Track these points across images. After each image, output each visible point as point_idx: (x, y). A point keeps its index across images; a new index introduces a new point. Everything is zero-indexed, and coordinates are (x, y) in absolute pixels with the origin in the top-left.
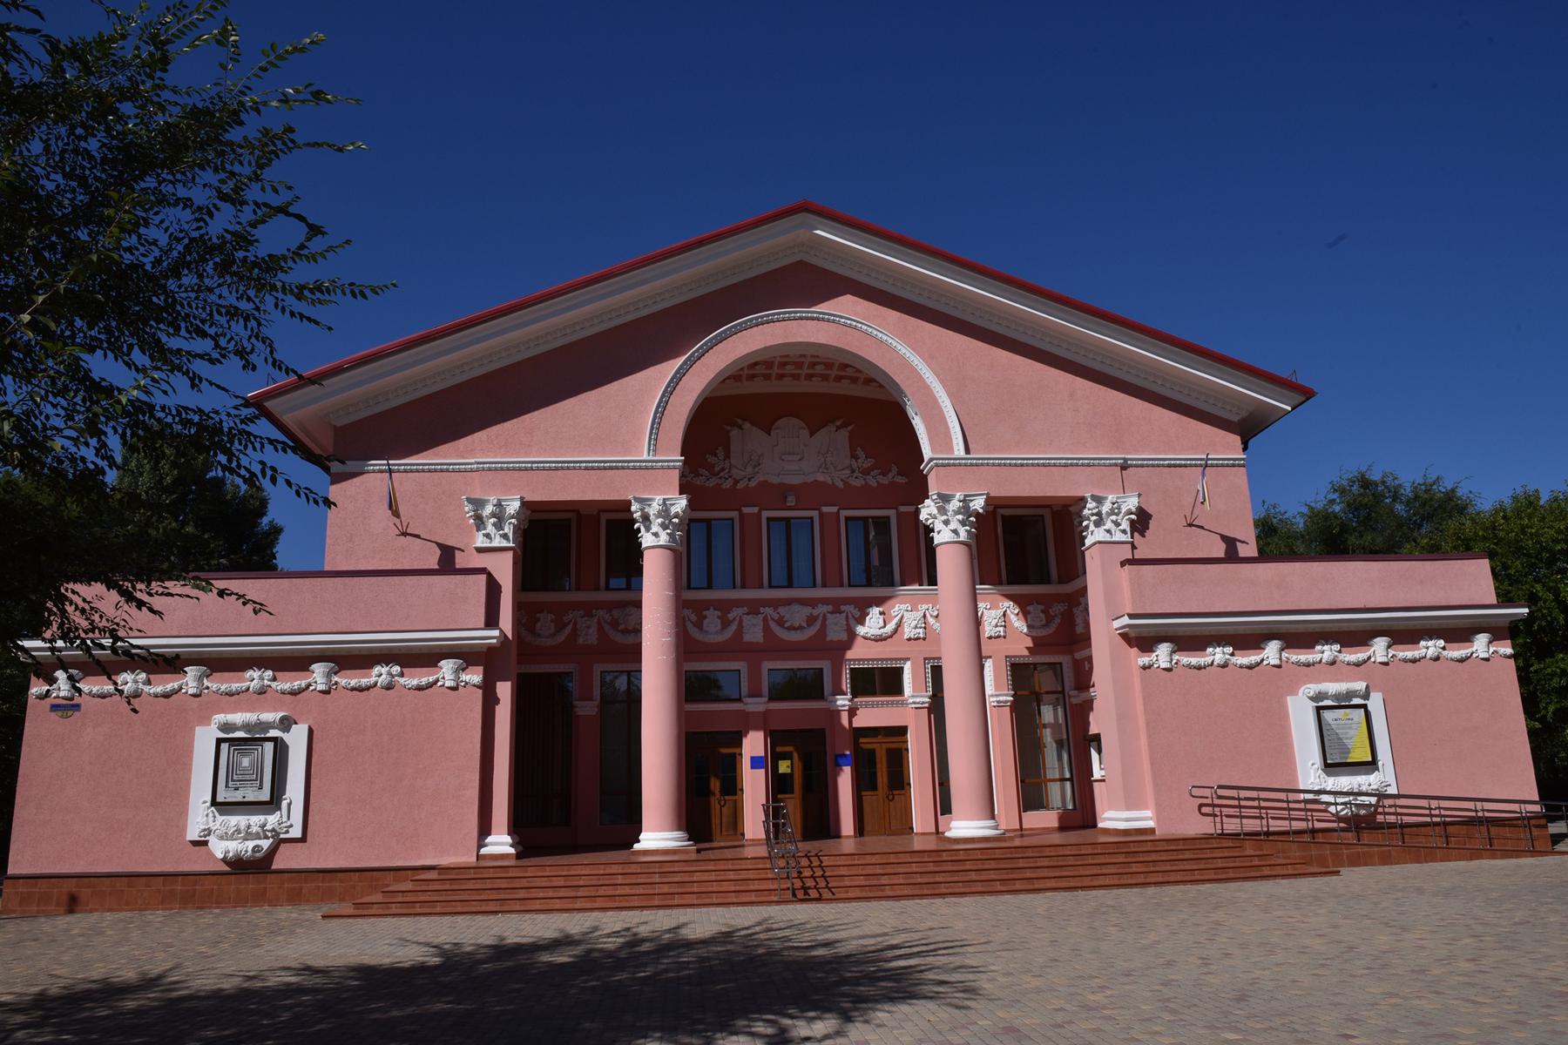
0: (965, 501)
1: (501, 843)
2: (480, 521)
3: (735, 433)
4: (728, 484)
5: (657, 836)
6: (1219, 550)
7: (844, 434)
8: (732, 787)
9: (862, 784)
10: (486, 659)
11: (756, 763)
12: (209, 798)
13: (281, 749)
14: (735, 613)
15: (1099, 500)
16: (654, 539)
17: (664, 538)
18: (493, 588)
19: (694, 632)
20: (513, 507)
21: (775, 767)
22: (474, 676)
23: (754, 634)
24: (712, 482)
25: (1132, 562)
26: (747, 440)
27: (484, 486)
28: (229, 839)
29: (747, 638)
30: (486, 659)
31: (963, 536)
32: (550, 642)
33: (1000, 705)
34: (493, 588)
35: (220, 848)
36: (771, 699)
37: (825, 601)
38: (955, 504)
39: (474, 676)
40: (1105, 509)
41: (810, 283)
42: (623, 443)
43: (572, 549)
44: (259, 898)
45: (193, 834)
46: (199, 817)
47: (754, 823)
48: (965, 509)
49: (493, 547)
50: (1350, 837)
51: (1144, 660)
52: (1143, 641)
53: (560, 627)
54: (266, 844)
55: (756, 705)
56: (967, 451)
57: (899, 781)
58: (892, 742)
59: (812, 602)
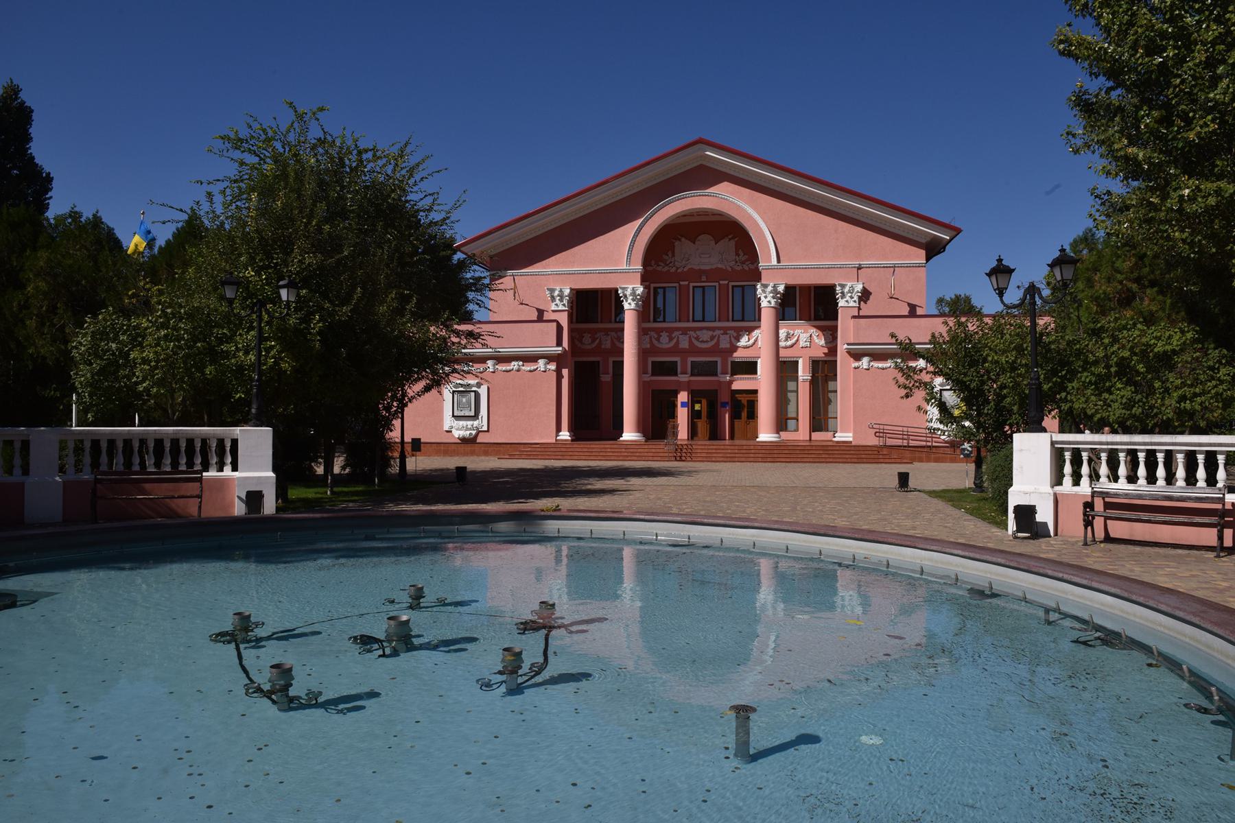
0: (775, 287)
1: (565, 435)
2: (553, 299)
3: (677, 243)
4: (673, 270)
5: (629, 435)
6: (906, 311)
7: (733, 243)
8: (673, 415)
9: (735, 416)
10: (558, 359)
11: (683, 404)
12: (731, 740)
13: (477, 396)
14: (676, 334)
15: (843, 286)
16: (629, 305)
17: (633, 306)
18: (559, 328)
19: (655, 342)
20: (567, 292)
21: (693, 407)
22: (553, 367)
23: (684, 344)
24: (666, 268)
25: (859, 317)
26: (683, 247)
27: (552, 283)
28: (460, 430)
29: (681, 346)
30: (558, 359)
31: (773, 304)
32: (589, 347)
33: (804, 381)
34: (559, 328)
35: (457, 434)
36: (692, 375)
37: (719, 328)
38: (770, 289)
39: (553, 367)
40: (846, 290)
41: (706, 176)
42: (614, 260)
43: (593, 307)
44: (472, 453)
45: (446, 428)
46: (448, 422)
47: (683, 433)
48: (775, 291)
49: (559, 309)
50: (949, 451)
51: (856, 364)
52: (857, 356)
53: (594, 340)
54: (474, 432)
55: (684, 378)
56: (779, 261)
57: (752, 414)
58: (750, 397)
59: (713, 329)
